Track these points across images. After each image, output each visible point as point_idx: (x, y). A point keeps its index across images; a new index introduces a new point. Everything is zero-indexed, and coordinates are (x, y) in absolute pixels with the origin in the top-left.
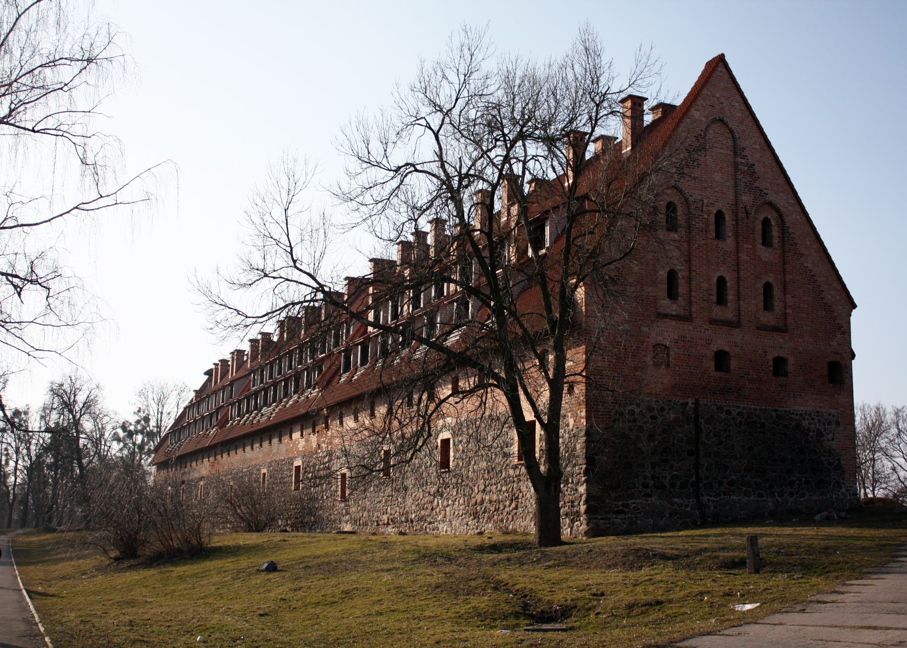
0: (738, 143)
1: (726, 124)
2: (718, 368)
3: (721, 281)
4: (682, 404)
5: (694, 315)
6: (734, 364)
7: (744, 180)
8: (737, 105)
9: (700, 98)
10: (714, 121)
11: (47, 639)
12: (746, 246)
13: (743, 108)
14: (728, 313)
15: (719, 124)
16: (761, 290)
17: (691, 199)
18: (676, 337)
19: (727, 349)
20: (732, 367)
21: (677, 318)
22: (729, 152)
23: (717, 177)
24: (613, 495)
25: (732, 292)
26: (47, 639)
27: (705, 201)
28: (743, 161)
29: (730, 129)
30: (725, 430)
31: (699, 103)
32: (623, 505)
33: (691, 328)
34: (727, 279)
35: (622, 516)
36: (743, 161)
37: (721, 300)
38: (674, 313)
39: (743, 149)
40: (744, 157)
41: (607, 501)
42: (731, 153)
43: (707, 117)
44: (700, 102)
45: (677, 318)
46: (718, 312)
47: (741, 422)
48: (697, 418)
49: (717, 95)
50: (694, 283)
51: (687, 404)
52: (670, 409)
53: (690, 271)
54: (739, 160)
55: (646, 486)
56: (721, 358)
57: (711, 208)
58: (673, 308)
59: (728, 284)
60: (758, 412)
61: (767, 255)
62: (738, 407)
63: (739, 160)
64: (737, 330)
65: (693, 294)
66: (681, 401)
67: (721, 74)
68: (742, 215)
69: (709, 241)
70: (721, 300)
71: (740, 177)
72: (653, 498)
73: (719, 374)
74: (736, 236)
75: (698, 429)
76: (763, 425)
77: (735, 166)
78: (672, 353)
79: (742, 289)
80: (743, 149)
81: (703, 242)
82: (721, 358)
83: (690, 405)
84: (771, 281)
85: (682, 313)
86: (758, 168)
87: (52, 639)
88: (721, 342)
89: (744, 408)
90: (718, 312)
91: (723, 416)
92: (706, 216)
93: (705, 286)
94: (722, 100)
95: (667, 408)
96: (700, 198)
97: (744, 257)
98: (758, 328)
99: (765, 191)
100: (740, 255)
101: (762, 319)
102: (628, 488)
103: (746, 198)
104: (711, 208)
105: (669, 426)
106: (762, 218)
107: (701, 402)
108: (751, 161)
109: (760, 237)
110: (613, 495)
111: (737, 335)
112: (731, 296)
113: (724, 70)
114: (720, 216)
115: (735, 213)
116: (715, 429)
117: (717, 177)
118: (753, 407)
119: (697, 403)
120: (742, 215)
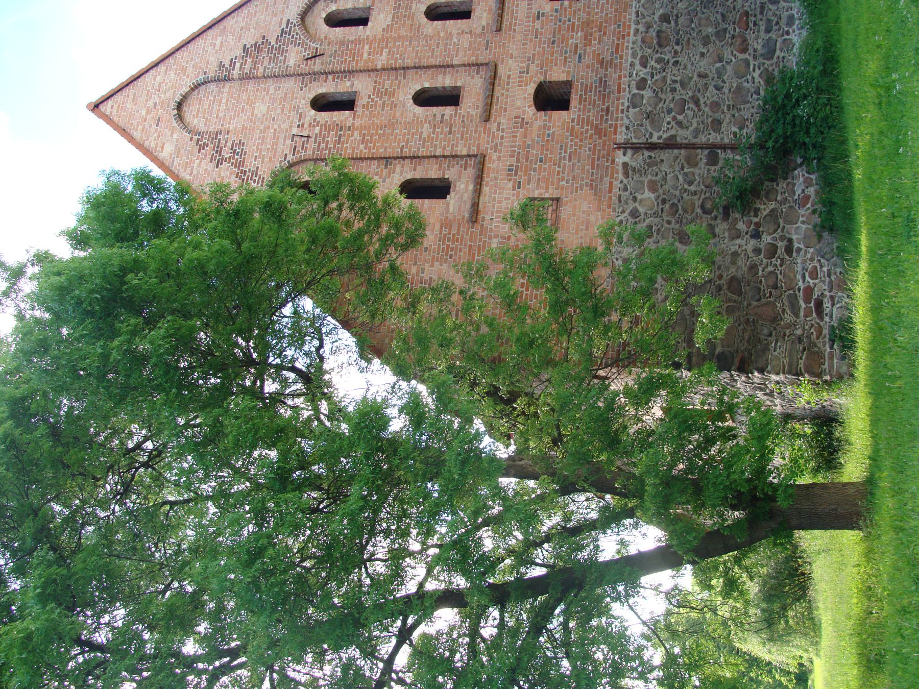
0: (211, 75)
1: (185, 97)
2: (562, 104)
3: (424, 99)
4: (626, 174)
5: (474, 150)
6: (558, 75)
7: (266, 63)
8: (159, 79)
9: (147, 144)
10: (180, 117)
11: (217, 664)
12: (365, 56)
13: (164, 68)
14: (473, 87)
15: (185, 108)
16: (438, 24)
17: (290, 157)
18: (510, 184)
19: (531, 89)
20: (563, 77)
21: (479, 180)
22: (226, 90)
23: (261, 108)
24: (789, 318)
25: (440, 78)
26: (217, 664)
27: (295, 131)
28: (238, 65)
29: (193, 90)
30: (673, 90)
31: (153, 145)
32: (807, 300)
33: (495, 156)
34: (418, 87)
35: (827, 304)
36: (238, 65)
37: (451, 98)
38: (471, 187)
39: (221, 65)
40: (232, 63)
41: (799, 332)
42: (228, 85)
43: (173, 130)
44: (151, 143)
45: (479, 180)
46: (471, 104)
47: (659, 61)
48: (652, 147)
49: (144, 112)
50: (423, 152)
51: (625, 165)
52: (635, 199)
53: (403, 158)
54: (236, 73)
55: (772, 251)
56: (550, 98)
57: (307, 120)
58: (463, 188)
59: (427, 85)
60: (641, 28)
61: (382, 16)
62: (632, 65)
63: (236, 73)
64: (501, 70)
65: (439, 152)
66: (621, 176)
67: (116, 106)
68: (317, 65)
69: (358, 123)
70: (451, 98)
71: (261, 70)
72: (794, 237)
73: (574, 102)
74: (351, 72)
75: (670, 144)
76: (665, 18)
77: (246, 78)
78: (536, 194)
79: (433, 62)
80: (221, 65)
81: (356, 133)
82: (550, 98)
83: (626, 159)
84: (424, 8)
85: (471, 172)
86: (250, 39)
87: (216, 659)
88: (519, 98)
89: (634, 55)
90: (471, 104)
91: (647, 93)
92: (317, 130)
93: (426, 130)
94: (150, 104)
95: (631, 206)
96: (289, 142)
97: (382, 60)
98: (499, 30)
99: (284, 26)
100: (379, 67)
101: (484, 23)
102: (775, 287)
103: (293, 58)
104: (307, 120)
105: (664, 201)
106: (325, 28)
107: (621, 138)
108: (239, 52)
109: (353, 29)
110: (789, 318)
111: (509, 68)
112: (445, 81)
113: (110, 102)
114: (322, 104)
115: (315, 75)
116: (669, 111)
117: (261, 108)
118: (632, 38)
119: (625, 147)
120: (317, 65)
